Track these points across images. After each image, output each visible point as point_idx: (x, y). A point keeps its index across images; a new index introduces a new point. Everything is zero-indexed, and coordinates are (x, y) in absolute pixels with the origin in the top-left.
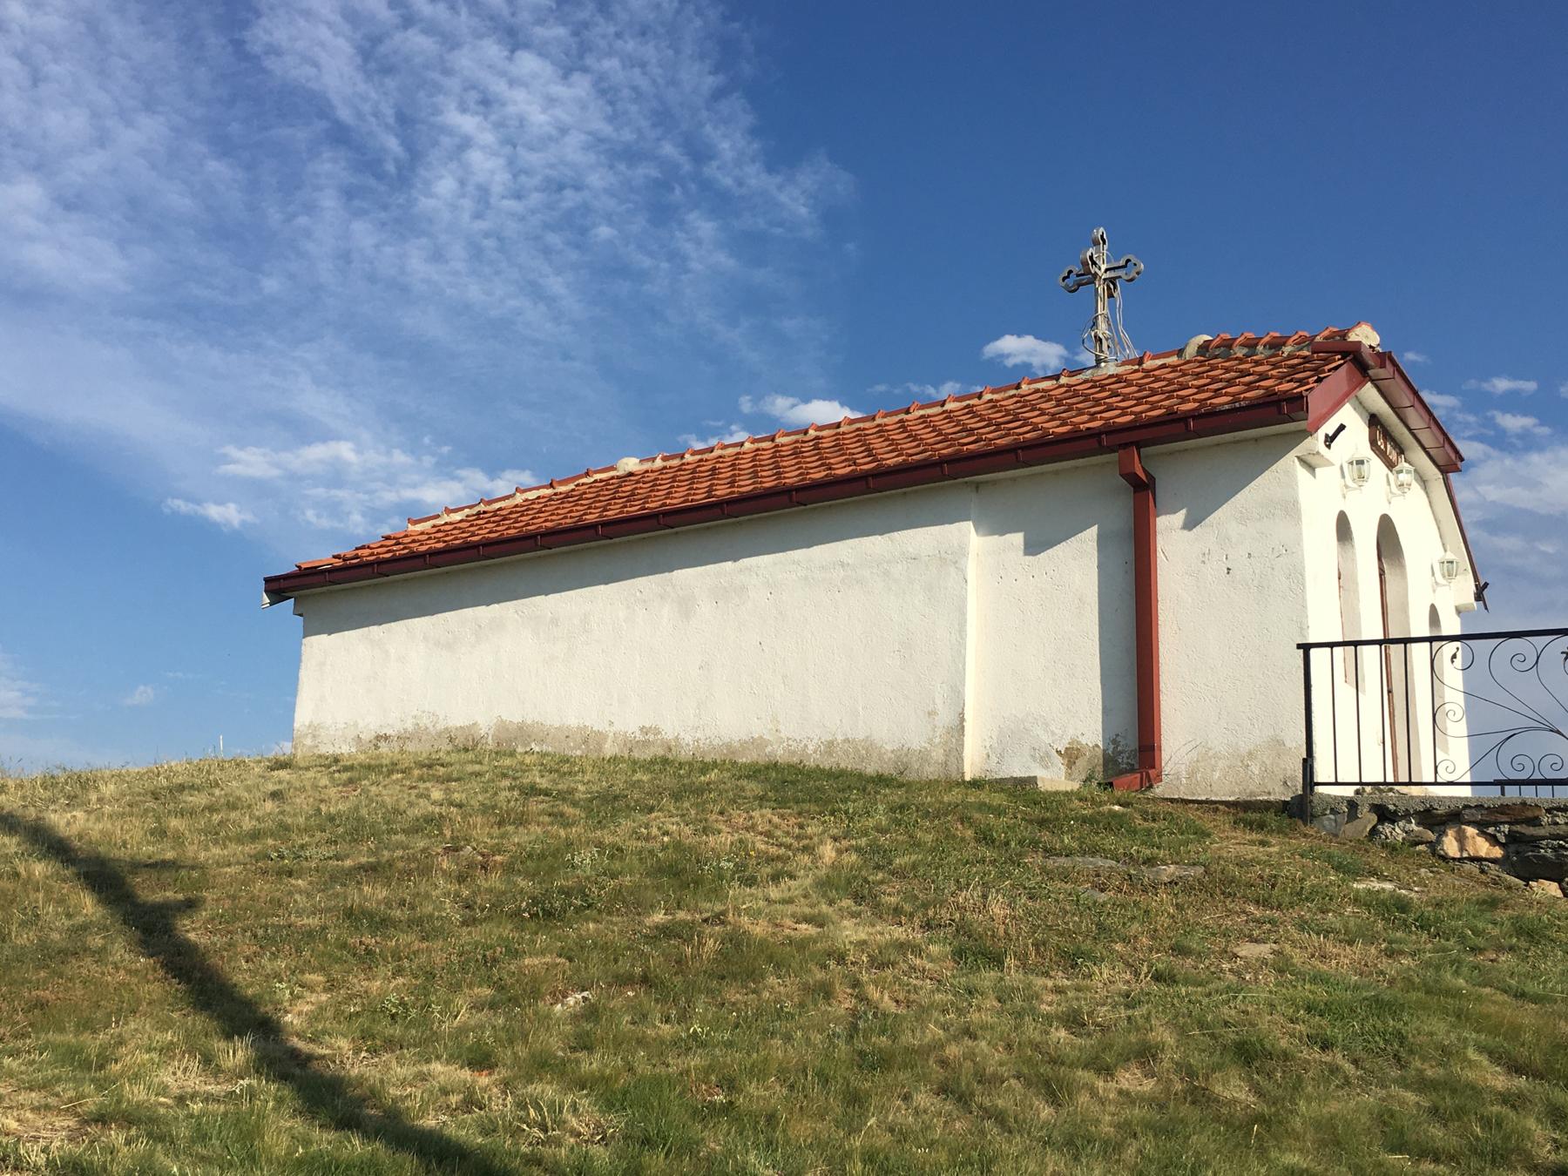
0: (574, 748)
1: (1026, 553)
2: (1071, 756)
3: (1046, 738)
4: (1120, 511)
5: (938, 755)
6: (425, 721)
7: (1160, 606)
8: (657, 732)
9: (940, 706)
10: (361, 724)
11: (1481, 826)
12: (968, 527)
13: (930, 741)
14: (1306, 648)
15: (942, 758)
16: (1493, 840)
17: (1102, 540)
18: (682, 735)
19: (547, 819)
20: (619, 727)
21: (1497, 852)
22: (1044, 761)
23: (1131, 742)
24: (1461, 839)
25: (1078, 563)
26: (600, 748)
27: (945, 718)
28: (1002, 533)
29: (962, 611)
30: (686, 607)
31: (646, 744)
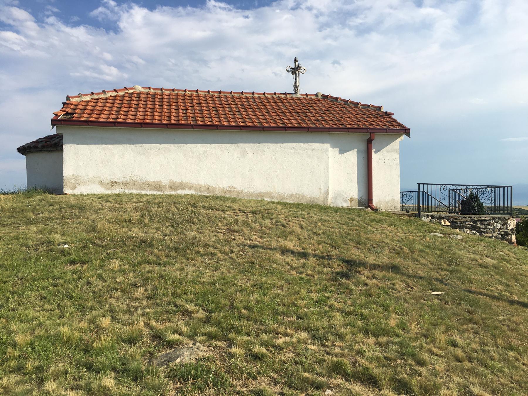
0: (204, 191)
1: (340, 153)
2: (351, 200)
3: (346, 196)
4: (363, 146)
5: (322, 199)
6: (135, 178)
7: (230, 147)
8: (235, 188)
9: (322, 188)
10: (102, 177)
11: (448, 220)
12: (327, 146)
13: (320, 196)
14: (419, 184)
15: (323, 200)
16: (449, 222)
17: (356, 153)
18: (244, 190)
19: (415, 231)
20: (221, 186)
21: (449, 224)
22: (345, 201)
23: (365, 198)
24: (445, 222)
25: (352, 158)
26: (213, 191)
27: (323, 190)
28: (333, 148)
29: (328, 165)
30: (244, 154)
31: (231, 191)
